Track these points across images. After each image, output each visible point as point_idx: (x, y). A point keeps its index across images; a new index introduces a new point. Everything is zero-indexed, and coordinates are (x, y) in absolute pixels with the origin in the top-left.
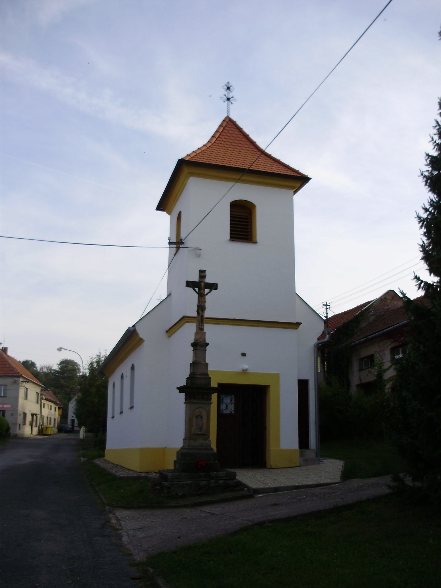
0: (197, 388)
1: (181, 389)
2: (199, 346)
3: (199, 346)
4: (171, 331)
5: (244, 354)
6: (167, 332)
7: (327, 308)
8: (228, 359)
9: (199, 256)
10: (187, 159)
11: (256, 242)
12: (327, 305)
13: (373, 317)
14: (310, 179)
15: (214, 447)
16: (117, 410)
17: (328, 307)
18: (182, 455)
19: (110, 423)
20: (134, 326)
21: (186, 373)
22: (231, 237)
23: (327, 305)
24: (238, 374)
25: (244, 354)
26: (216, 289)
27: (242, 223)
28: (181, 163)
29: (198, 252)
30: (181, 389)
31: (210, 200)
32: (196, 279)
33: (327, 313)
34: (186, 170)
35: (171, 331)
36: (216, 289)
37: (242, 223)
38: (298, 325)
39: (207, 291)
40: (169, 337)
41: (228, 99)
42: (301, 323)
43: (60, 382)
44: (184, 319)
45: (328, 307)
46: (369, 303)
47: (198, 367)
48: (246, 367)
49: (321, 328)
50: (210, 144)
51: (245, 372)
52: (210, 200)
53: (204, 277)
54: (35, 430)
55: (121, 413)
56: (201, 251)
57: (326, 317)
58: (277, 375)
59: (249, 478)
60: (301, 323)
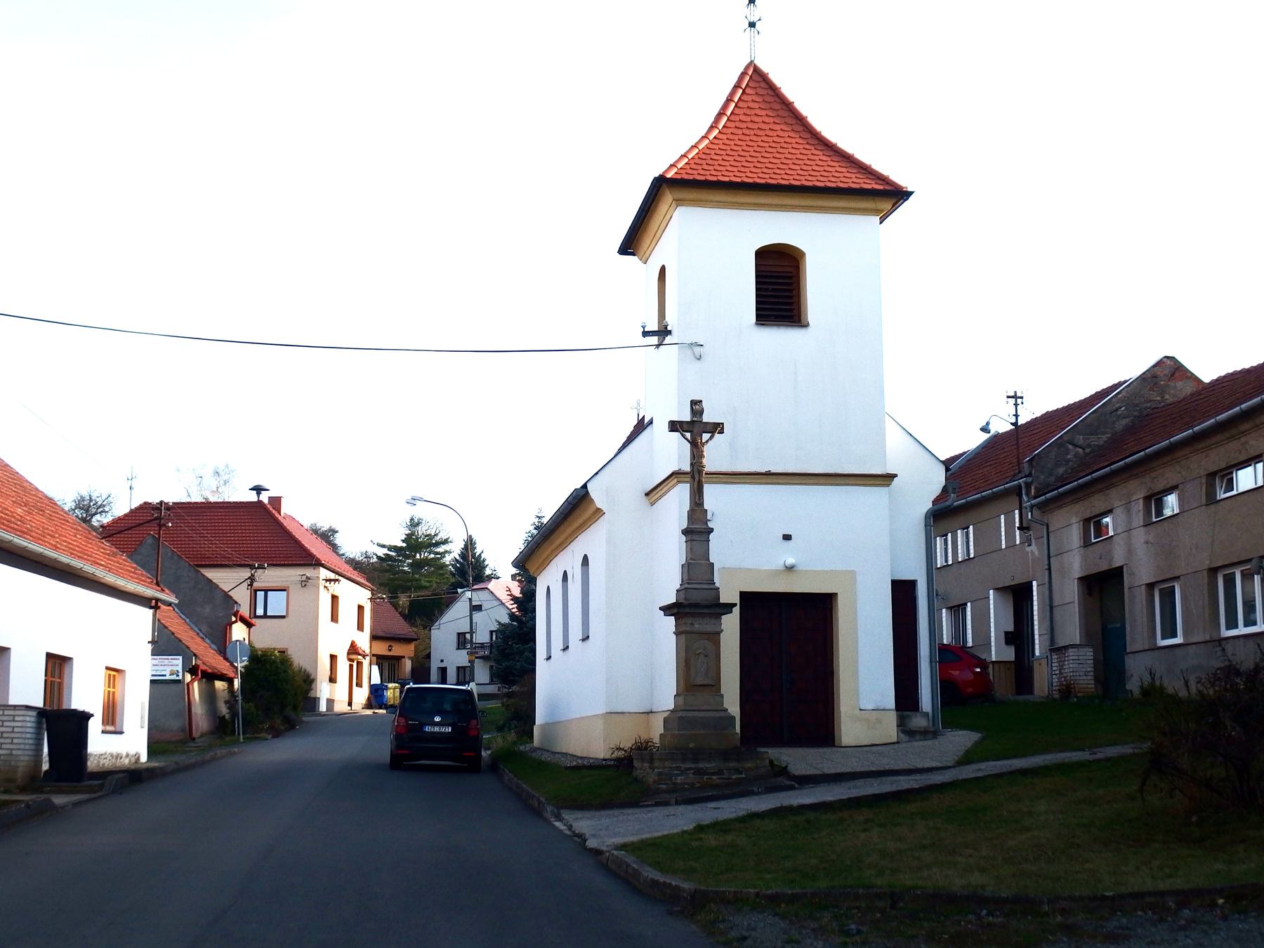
0: (694, 608)
1: (667, 610)
2: (698, 531)
3: (698, 531)
4: (653, 493)
5: (787, 537)
6: (647, 495)
7: (1016, 405)
8: (759, 546)
9: (583, 640)
10: (669, 176)
11: (806, 325)
12: (1015, 397)
13: (1124, 422)
14: (912, 193)
15: (732, 704)
16: (557, 643)
17: (1019, 401)
18: (675, 720)
19: (543, 670)
20: (585, 486)
21: (676, 582)
22: (757, 316)
23: (1015, 397)
24: (775, 573)
25: (787, 537)
26: (721, 432)
27: (780, 289)
28: (660, 185)
29: (697, 350)
30: (667, 610)
31: (716, 248)
32: (687, 417)
33: (1016, 416)
34: (668, 197)
35: (653, 493)
36: (721, 432)
37: (780, 289)
38: (888, 478)
39: (706, 436)
40: (652, 504)
41: (752, 25)
42: (896, 476)
43: (415, 582)
44: (676, 475)
45: (1019, 401)
46: (1120, 384)
47: (698, 566)
48: (790, 561)
49: (938, 479)
50: (716, 132)
51: (790, 568)
52: (716, 248)
53: (702, 412)
54: (361, 695)
55: (566, 648)
56: (702, 349)
57: (1015, 424)
58: (852, 574)
59: (800, 760)
60: (896, 476)
